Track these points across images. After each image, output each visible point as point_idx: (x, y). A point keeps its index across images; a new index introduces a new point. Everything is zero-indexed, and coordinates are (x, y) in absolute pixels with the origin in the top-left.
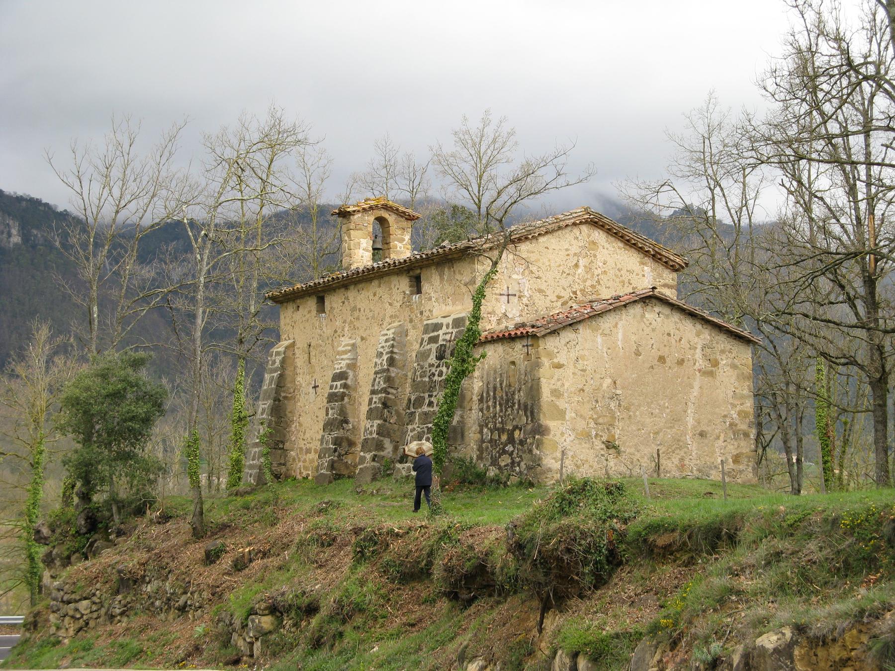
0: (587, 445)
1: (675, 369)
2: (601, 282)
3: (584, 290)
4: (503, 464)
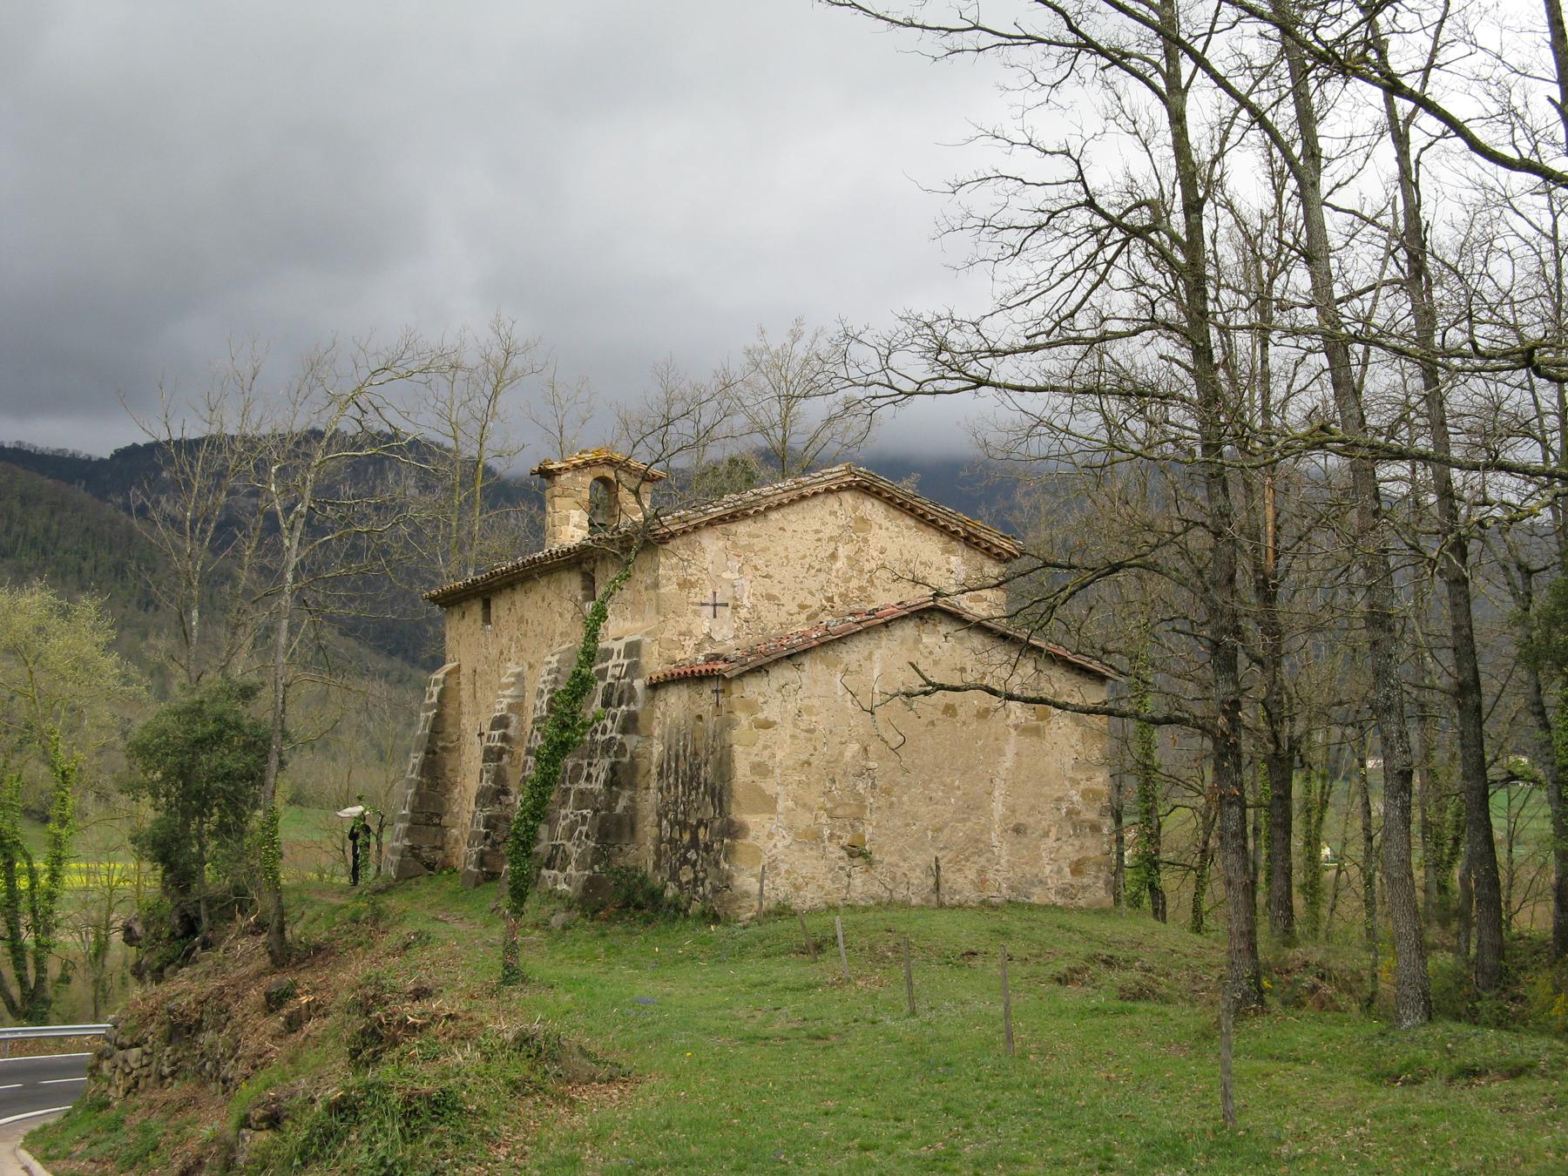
0: (814, 853)
1: (974, 726)
3: (847, 596)
4: (684, 879)
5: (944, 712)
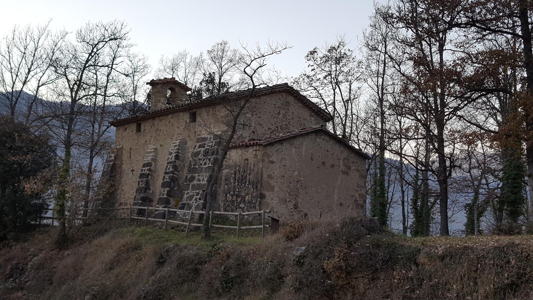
0: (284, 206)
1: (330, 169)
2: (290, 123)
5: (322, 164)
